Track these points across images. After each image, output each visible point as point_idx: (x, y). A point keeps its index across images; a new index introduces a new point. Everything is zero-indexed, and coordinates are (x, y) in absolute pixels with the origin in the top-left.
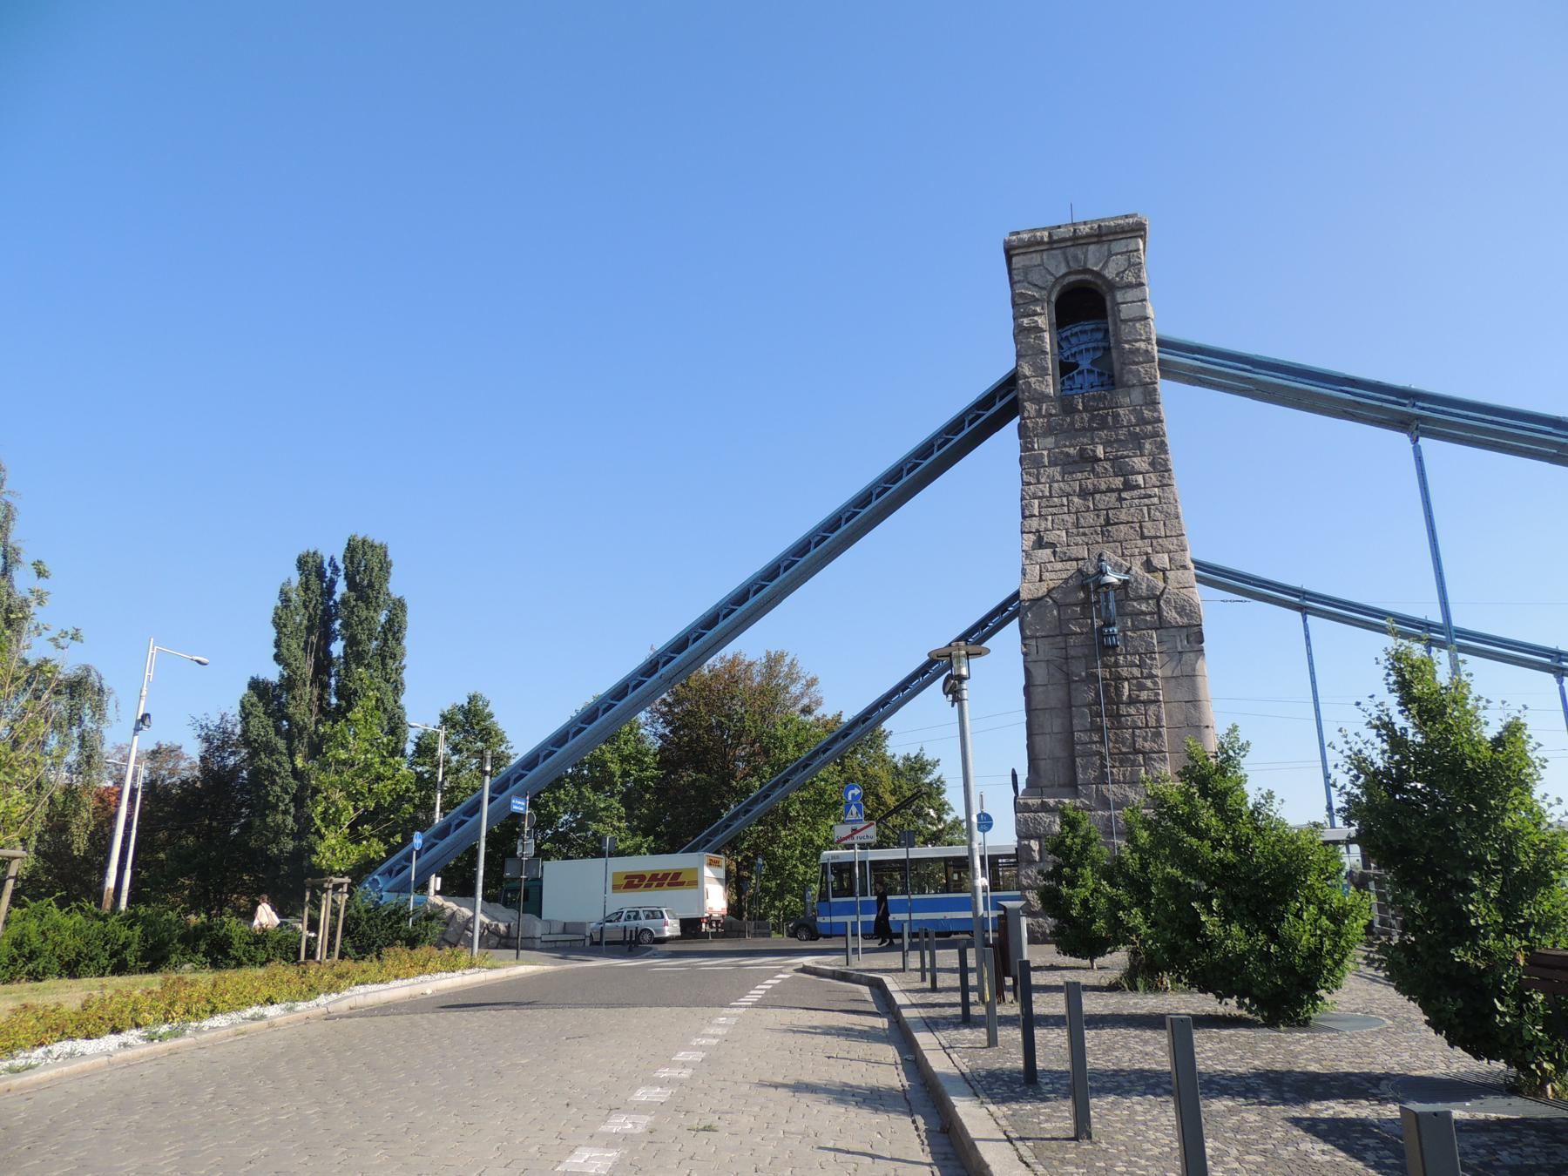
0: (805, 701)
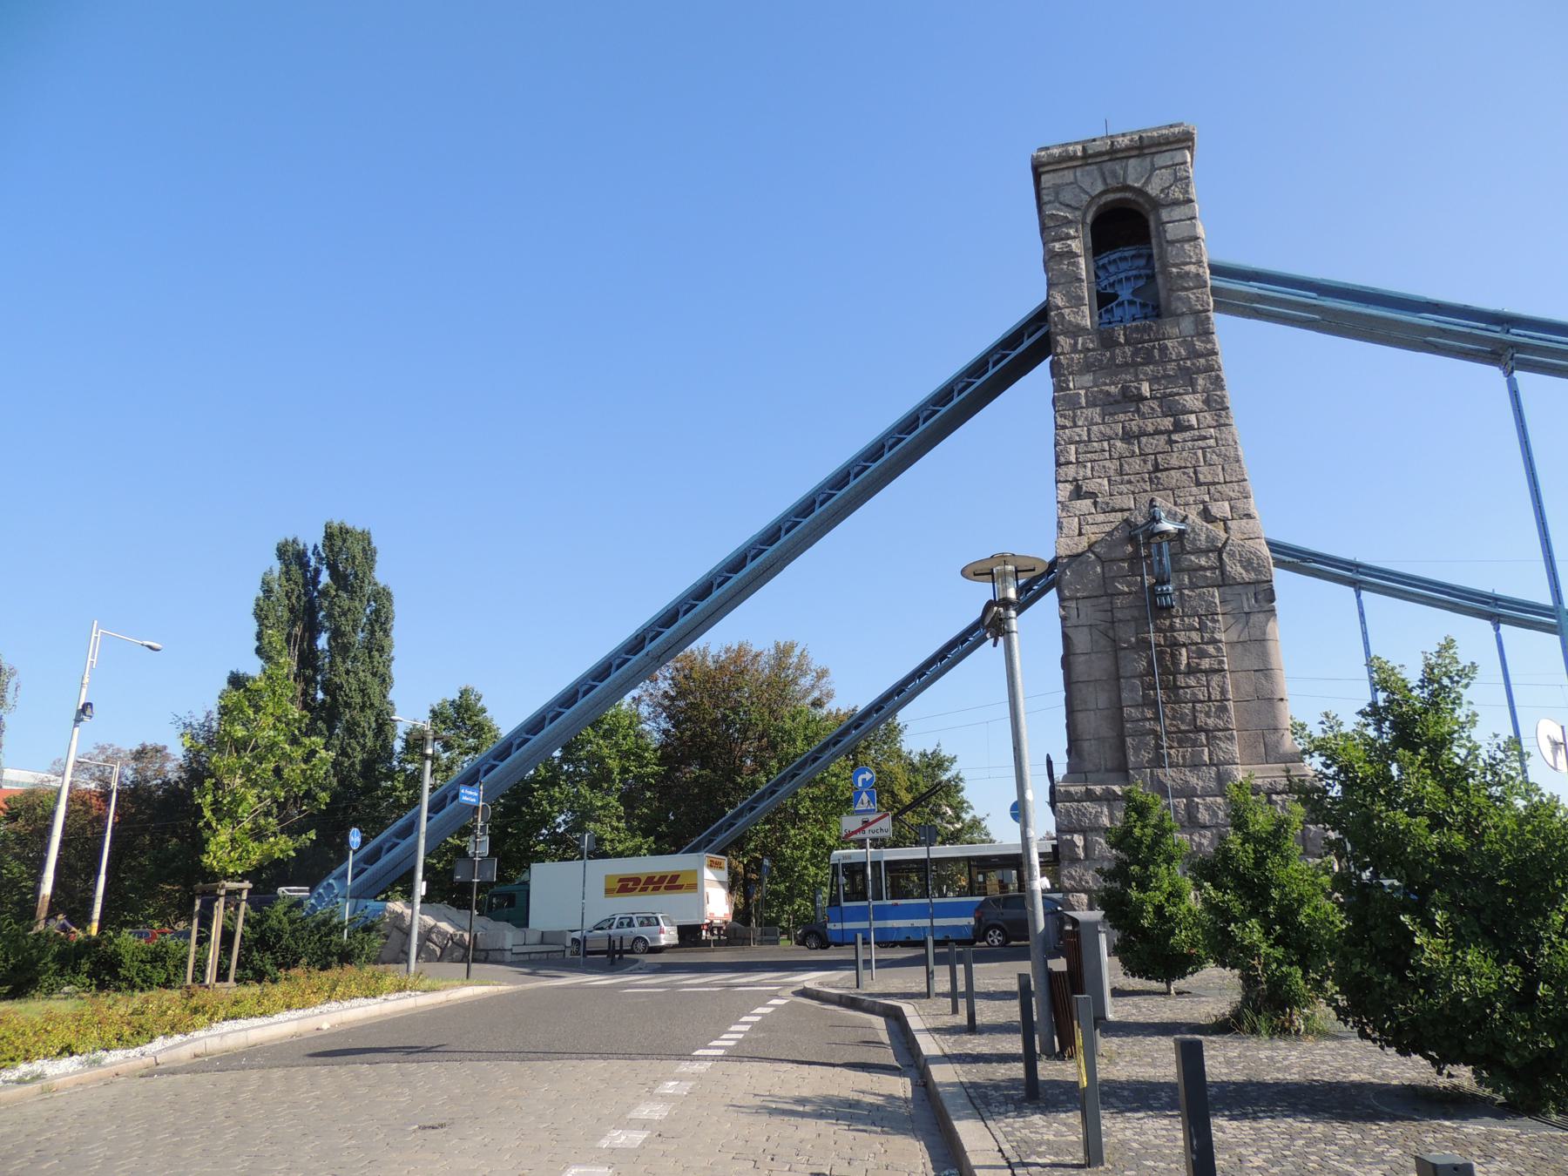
0: (816, 694)
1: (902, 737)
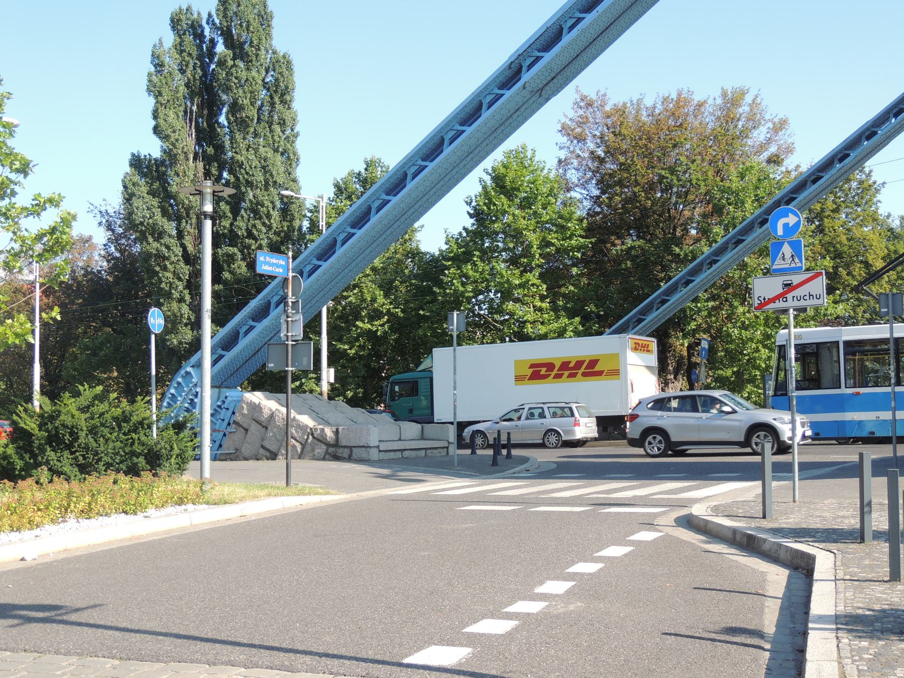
0: (773, 149)
1: (879, 197)
